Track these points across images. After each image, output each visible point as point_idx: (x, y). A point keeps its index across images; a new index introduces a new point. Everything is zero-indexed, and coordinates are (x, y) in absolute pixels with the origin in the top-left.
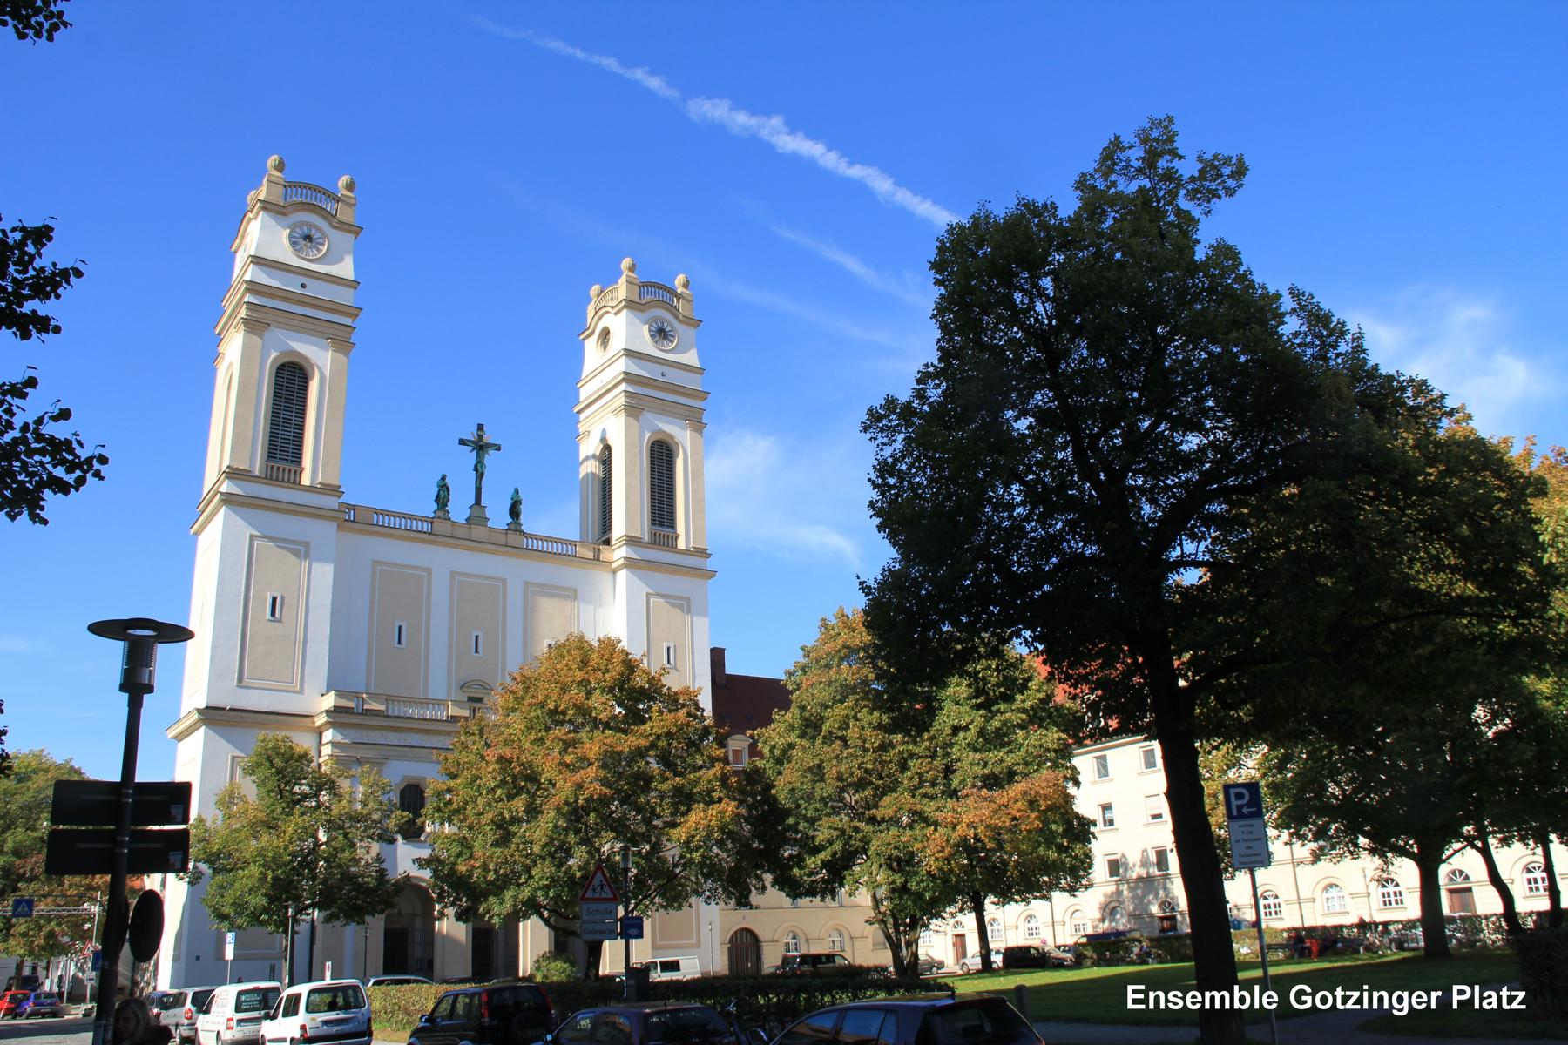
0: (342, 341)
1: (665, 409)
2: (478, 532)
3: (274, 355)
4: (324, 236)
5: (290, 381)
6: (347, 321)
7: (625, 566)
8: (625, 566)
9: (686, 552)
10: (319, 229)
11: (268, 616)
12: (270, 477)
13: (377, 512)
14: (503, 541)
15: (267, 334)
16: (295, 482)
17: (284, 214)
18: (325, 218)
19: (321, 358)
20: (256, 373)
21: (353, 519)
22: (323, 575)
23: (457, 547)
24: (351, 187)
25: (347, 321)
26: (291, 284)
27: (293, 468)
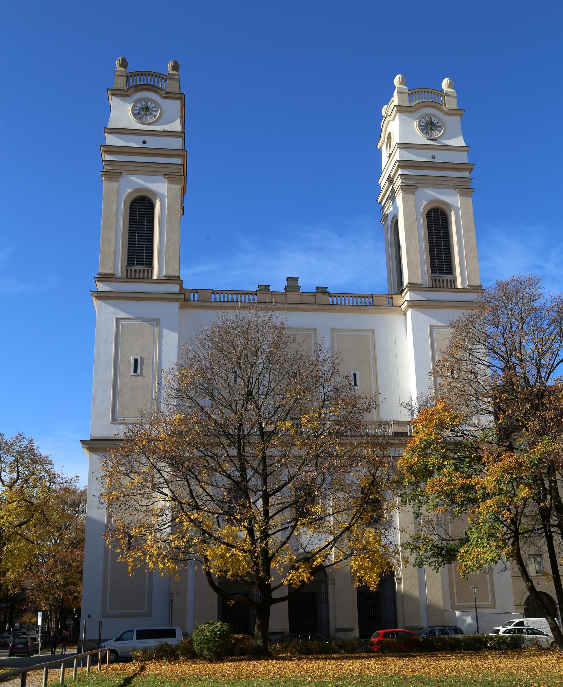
0: (465, 189)
1: (435, 183)
2: (293, 297)
3: (425, 203)
4: (158, 106)
5: (437, 222)
6: (466, 174)
7: (410, 306)
8: (410, 306)
9: (463, 290)
10: (153, 101)
11: (132, 372)
12: (436, 286)
13: (213, 292)
14: (313, 302)
15: (121, 180)
16: (149, 279)
17: (128, 96)
18: (157, 92)
19: (455, 201)
20: (115, 207)
21: (187, 299)
22: (171, 341)
23: (305, 310)
24: (176, 67)
25: (466, 174)
26: (424, 157)
27: (146, 269)
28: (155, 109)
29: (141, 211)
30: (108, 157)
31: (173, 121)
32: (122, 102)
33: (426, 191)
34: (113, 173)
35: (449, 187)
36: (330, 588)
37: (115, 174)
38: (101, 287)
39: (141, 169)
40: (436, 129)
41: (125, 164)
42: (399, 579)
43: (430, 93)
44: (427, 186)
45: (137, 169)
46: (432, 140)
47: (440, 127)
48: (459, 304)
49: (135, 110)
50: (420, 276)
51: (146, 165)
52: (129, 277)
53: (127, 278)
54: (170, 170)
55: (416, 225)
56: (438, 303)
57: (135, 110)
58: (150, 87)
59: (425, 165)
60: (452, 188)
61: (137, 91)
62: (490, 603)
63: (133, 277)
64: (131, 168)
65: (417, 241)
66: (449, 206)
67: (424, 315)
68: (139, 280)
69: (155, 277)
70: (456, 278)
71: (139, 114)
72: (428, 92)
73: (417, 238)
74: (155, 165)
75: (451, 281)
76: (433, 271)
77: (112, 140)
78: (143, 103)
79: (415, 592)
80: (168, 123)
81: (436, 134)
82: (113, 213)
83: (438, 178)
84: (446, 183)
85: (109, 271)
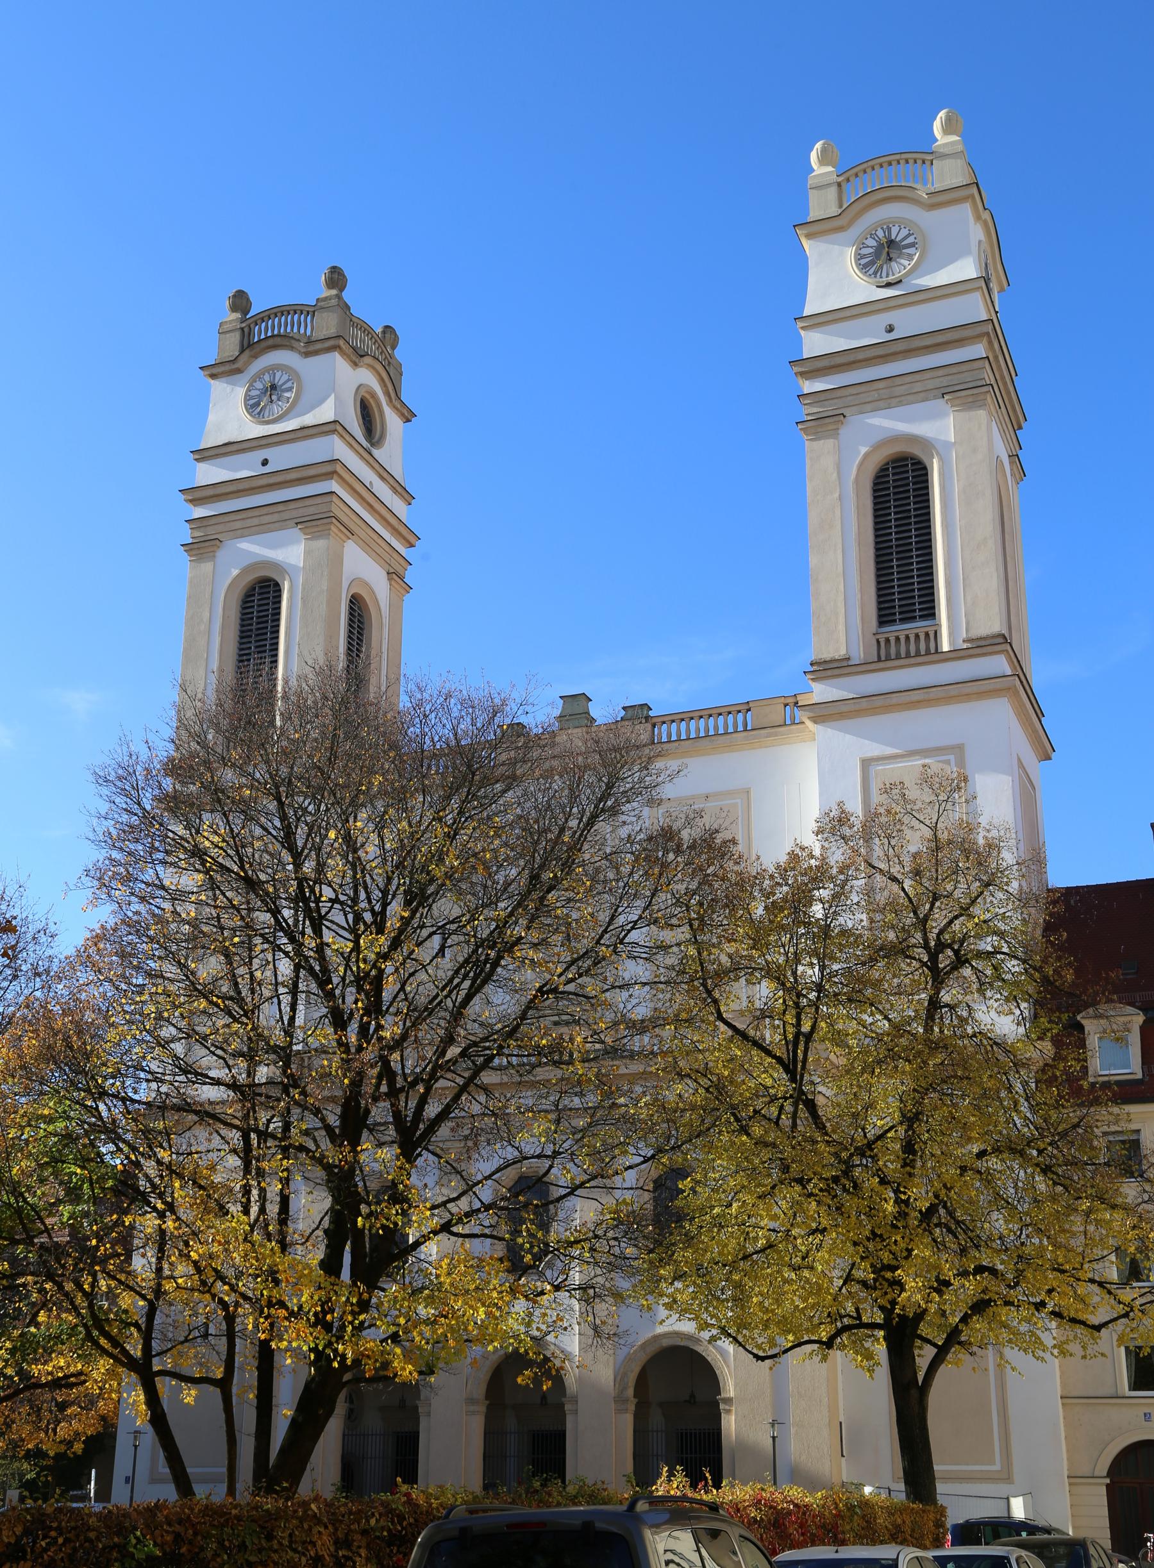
1: (890, 394)
4: (294, 375)
15: (844, 431)
17: (239, 371)
28: (289, 384)
29: (900, 494)
30: (809, 387)
31: (321, 401)
32: (229, 388)
33: (869, 421)
34: (826, 419)
35: (925, 395)
36: (569, 1419)
37: (207, 544)
38: (821, 692)
39: (256, 521)
40: (900, 256)
41: (227, 518)
42: (729, 1401)
43: (894, 163)
44: (868, 407)
45: (249, 523)
46: (888, 285)
47: (913, 245)
48: (895, 699)
49: (863, 257)
50: (843, 639)
51: (265, 510)
52: (885, 655)
53: (879, 660)
54: (312, 510)
55: (838, 513)
56: (879, 701)
57: (863, 257)
58: (278, 341)
59: (861, 356)
60: (935, 398)
61: (256, 357)
62: (997, 1467)
63: (923, 653)
64: (238, 525)
65: (839, 552)
66: (925, 443)
67: (848, 736)
68: (919, 660)
69: (945, 647)
70: (939, 625)
71: (872, 263)
72: (907, 162)
73: (840, 546)
74: (280, 508)
75: (927, 635)
76: (885, 617)
77: (816, 343)
78: (267, 377)
79: (762, 1437)
80: (313, 407)
81: (900, 267)
82: (202, 627)
83: (898, 381)
84: (918, 387)
85: (836, 649)
